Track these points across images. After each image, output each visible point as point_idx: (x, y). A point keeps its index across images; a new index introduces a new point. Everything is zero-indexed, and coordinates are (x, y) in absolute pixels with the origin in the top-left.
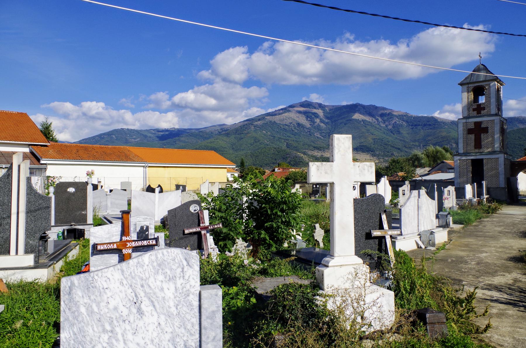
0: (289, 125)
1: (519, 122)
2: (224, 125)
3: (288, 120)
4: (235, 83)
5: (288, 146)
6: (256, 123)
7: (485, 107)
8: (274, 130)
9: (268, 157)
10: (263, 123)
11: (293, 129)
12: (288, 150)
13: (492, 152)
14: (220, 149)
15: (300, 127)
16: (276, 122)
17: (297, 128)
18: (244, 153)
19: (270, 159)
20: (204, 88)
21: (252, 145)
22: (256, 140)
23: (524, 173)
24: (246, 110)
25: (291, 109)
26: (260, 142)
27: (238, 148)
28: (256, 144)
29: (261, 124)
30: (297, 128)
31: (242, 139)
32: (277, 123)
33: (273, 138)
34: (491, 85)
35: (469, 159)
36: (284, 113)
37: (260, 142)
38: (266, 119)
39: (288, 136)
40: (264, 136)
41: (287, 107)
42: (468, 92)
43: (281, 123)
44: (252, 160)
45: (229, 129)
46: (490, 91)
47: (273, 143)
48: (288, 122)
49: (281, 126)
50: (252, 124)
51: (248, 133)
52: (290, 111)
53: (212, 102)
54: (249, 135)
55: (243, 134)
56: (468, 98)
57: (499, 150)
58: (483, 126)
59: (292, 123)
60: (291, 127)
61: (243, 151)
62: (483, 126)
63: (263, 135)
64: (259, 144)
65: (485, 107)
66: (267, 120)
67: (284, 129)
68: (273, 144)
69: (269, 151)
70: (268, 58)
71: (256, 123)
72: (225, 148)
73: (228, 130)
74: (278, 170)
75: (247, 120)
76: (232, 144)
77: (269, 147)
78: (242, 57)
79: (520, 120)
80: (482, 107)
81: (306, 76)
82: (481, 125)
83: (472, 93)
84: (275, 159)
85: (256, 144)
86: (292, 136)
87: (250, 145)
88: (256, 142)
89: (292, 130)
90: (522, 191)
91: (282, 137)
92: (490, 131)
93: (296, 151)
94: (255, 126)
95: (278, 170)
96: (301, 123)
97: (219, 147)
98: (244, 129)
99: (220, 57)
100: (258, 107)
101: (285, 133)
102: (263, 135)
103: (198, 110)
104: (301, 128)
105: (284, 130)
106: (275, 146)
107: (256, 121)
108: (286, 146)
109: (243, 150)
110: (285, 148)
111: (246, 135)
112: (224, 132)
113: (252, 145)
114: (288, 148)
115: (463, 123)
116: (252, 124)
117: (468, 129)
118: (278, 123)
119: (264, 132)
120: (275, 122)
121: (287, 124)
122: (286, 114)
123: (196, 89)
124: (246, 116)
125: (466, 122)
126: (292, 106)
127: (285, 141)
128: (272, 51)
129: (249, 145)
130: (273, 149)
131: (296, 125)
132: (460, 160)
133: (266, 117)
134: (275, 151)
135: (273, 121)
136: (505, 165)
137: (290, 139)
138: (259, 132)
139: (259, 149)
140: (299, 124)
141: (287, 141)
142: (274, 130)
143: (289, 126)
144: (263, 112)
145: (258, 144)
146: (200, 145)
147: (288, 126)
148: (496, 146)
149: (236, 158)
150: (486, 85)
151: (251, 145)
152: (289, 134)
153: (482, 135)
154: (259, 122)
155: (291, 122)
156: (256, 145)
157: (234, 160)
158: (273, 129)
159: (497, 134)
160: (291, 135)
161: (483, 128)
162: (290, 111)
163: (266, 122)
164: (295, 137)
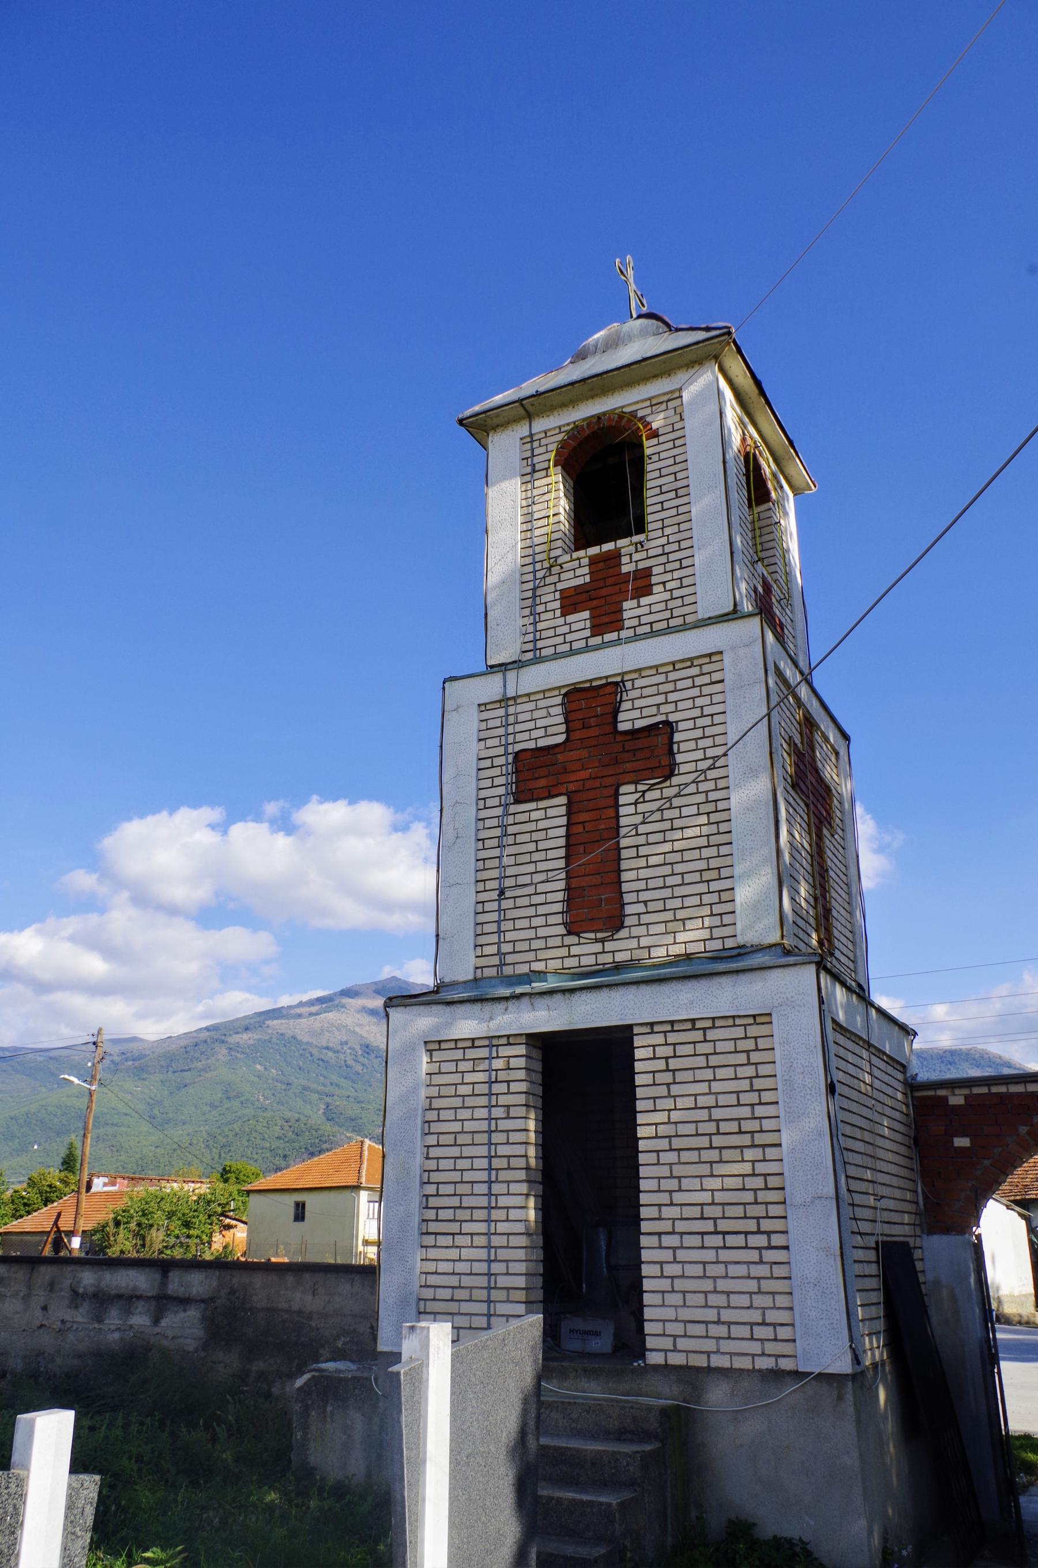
0: (339, 1048)
1: (972, 1064)
2: (134, 1039)
3: (337, 1033)
4: (172, 910)
5: (330, 1114)
6: (234, 1039)
7: (647, 573)
8: (289, 1064)
9: (263, 1148)
10: (259, 1040)
11: (349, 1062)
12: (328, 1128)
13: (717, 958)
14: (108, 1116)
15: (373, 1055)
16: (299, 1038)
17: (361, 1059)
18: (185, 1132)
19: (268, 1155)
20: (72, 924)
21: (216, 1107)
22: (229, 1093)
23: (1008, 1207)
24: (211, 998)
25: (346, 1000)
26: (242, 1099)
27: (171, 1115)
28: (229, 1105)
29: (251, 1042)
30: (361, 1059)
31: (186, 1086)
32: (300, 1043)
33: (284, 1087)
34: (686, 395)
35: (510, 1040)
36: (325, 1012)
37: (242, 1099)
38: (268, 1027)
39: (331, 1084)
40: (256, 1080)
41: (335, 994)
42: (532, 472)
43: (315, 1043)
44: (208, 1156)
45: (148, 1052)
46: (678, 441)
47: (283, 1105)
48: (334, 1039)
49: (315, 1051)
50: (223, 1042)
51: (207, 1069)
52: (343, 1006)
53: (95, 966)
54: (208, 1075)
55: (189, 1070)
56: (529, 519)
57: (774, 937)
58: (628, 719)
59: (346, 1043)
60: (342, 1056)
61: (185, 1127)
62: (628, 719)
63: (252, 1078)
64: (239, 1105)
65: (647, 573)
66: (270, 1031)
67: (323, 1060)
68: (282, 1107)
69: (268, 1128)
70: (282, 841)
71: (234, 1039)
72: (126, 1115)
73: (146, 1055)
74: (105, 1185)
75: (207, 1029)
76: (152, 1102)
77: (268, 1114)
78: (206, 838)
79: (974, 1059)
80: (625, 569)
81: (388, 906)
82: (616, 711)
83: (556, 478)
84: (285, 1156)
85: (229, 1105)
86: (343, 1082)
87: (209, 1109)
88: (228, 1098)
89: (347, 1066)
90: (1012, 1296)
91: (314, 1086)
92: (686, 758)
93: (354, 1131)
94: (230, 1049)
95: (105, 1185)
96: (375, 1044)
97: (106, 1110)
98: (197, 1055)
99: (134, 829)
100: (248, 989)
101: (324, 1072)
102: (252, 1078)
103: (42, 987)
104: (374, 1061)
105: (321, 1063)
106: (288, 1114)
107: (237, 1033)
108: (324, 1113)
109: (184, 1124)
110: (319, 1122)
111: (200, 1076)
112: (130, 1063)
113: (216, 1107)
114: (328, 1119)
115: (483, 707)
116: (223, 1042)
117: (517, 755)
118: (305, 1040)
119: (259, 1067)
120: (294, 1038)
121: (331, 1045)
122: (331, 1016)
123: (51, 922)
124: (205, 1016)
125: (505, 701)
126: (349, 993)
127: (320, 1099)
128: (285, 825)
129: (205, 1108)
130: (279, 1122)
131: (357, 1047)
132: (434, 1046)
133: (269, 1022)
134: (287, 1128)
135: (290, 1033)
136: (831, 1089)
137: (337, 1091)
138: (241, 1067)
139: (234, 1121)
140: (367, 1046)
141: (328, 1100)
142: (289, 1064)
143: (338, 1052)
144: (263, 1004)
145: (236, 1104)
146: (44, 1103)
147: (335, 1052)
148: (745, 894)
149: (158, 1150)
150: (654, 403)
151: (214, 1107)
152: (334, 1078)
153: (627, 794)
154: (245, 1036)
155: (345, 1039)
156: (228, 1109)
157: (151, 1154)
158: (289, 1059)
159: (752, 773)
160: (342, 1080)
161: (633, 733)
162: (343, 1006)
163: (266, 1037)
164: (355, 1086)
